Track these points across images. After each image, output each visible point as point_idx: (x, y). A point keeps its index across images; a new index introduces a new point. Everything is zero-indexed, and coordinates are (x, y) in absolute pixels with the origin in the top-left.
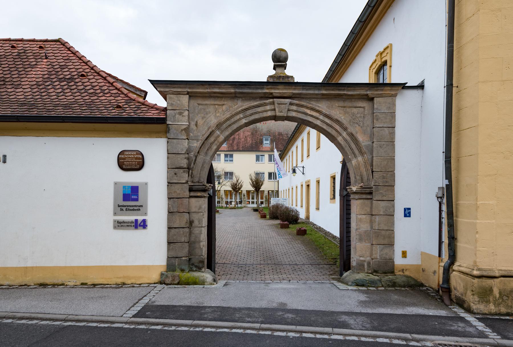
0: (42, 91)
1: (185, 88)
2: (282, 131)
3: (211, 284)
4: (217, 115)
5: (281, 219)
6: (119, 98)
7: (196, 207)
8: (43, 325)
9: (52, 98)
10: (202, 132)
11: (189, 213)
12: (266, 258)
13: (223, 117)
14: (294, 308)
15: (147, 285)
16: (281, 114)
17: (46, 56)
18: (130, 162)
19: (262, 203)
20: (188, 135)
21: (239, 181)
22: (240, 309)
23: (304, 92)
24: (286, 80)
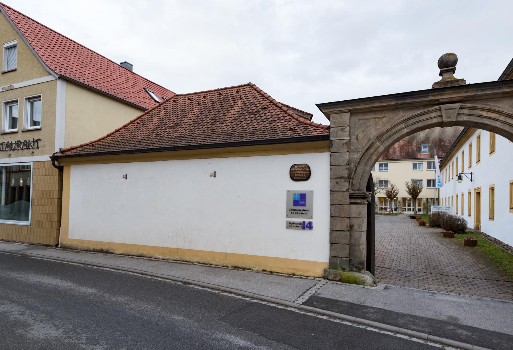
0: (238, 123)
1: (347, 106)
2: (444, 137)
3: (371, 286)
4: (378, 127)
5: (444, 228)
6: (291, 122)
7: (356, 213)
8: (238, 299)
9: (245, 128)
10: (364, 144)
11: (349, 218)
12: (428, 267)
13: (384, 128)
14: (468, 324)
15: (312, 278)
16: (449, 120)
17: (199, 103)
18: (300, 174)
19: (420, 210)
20: (349, 148)
21: (395, 189)
22: (404, 315)
23: (479, 93)
24: (456, 84)
